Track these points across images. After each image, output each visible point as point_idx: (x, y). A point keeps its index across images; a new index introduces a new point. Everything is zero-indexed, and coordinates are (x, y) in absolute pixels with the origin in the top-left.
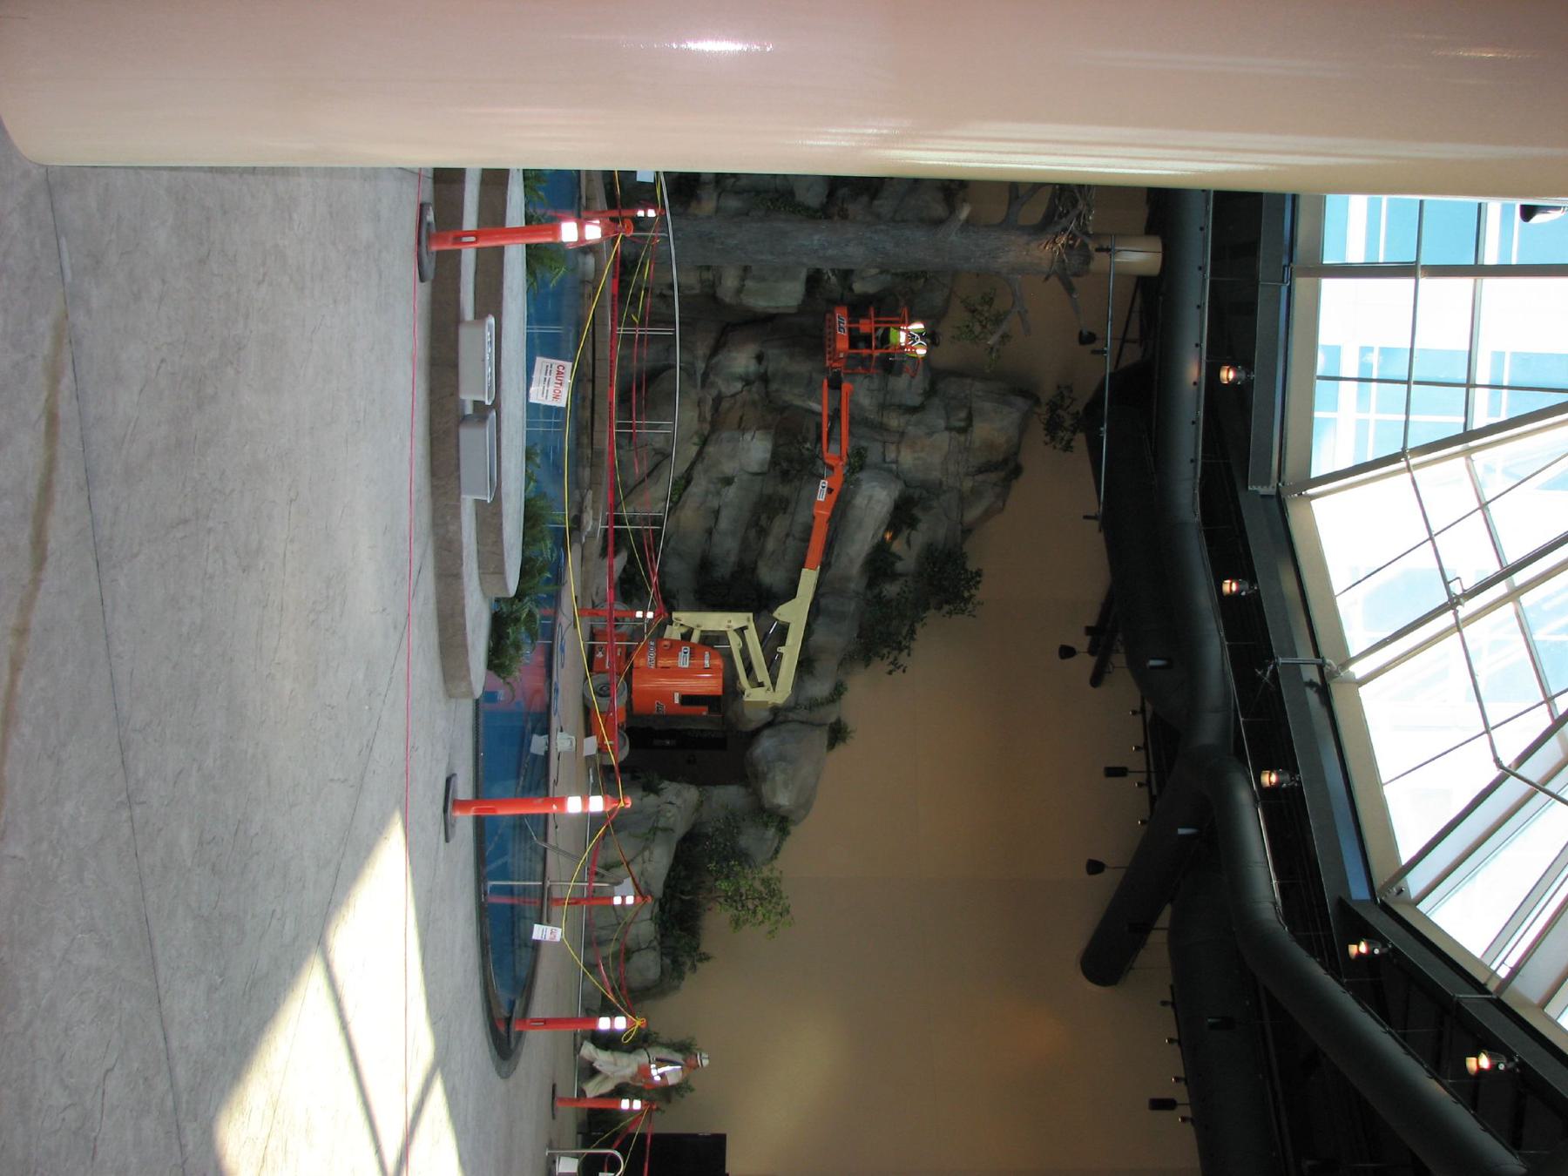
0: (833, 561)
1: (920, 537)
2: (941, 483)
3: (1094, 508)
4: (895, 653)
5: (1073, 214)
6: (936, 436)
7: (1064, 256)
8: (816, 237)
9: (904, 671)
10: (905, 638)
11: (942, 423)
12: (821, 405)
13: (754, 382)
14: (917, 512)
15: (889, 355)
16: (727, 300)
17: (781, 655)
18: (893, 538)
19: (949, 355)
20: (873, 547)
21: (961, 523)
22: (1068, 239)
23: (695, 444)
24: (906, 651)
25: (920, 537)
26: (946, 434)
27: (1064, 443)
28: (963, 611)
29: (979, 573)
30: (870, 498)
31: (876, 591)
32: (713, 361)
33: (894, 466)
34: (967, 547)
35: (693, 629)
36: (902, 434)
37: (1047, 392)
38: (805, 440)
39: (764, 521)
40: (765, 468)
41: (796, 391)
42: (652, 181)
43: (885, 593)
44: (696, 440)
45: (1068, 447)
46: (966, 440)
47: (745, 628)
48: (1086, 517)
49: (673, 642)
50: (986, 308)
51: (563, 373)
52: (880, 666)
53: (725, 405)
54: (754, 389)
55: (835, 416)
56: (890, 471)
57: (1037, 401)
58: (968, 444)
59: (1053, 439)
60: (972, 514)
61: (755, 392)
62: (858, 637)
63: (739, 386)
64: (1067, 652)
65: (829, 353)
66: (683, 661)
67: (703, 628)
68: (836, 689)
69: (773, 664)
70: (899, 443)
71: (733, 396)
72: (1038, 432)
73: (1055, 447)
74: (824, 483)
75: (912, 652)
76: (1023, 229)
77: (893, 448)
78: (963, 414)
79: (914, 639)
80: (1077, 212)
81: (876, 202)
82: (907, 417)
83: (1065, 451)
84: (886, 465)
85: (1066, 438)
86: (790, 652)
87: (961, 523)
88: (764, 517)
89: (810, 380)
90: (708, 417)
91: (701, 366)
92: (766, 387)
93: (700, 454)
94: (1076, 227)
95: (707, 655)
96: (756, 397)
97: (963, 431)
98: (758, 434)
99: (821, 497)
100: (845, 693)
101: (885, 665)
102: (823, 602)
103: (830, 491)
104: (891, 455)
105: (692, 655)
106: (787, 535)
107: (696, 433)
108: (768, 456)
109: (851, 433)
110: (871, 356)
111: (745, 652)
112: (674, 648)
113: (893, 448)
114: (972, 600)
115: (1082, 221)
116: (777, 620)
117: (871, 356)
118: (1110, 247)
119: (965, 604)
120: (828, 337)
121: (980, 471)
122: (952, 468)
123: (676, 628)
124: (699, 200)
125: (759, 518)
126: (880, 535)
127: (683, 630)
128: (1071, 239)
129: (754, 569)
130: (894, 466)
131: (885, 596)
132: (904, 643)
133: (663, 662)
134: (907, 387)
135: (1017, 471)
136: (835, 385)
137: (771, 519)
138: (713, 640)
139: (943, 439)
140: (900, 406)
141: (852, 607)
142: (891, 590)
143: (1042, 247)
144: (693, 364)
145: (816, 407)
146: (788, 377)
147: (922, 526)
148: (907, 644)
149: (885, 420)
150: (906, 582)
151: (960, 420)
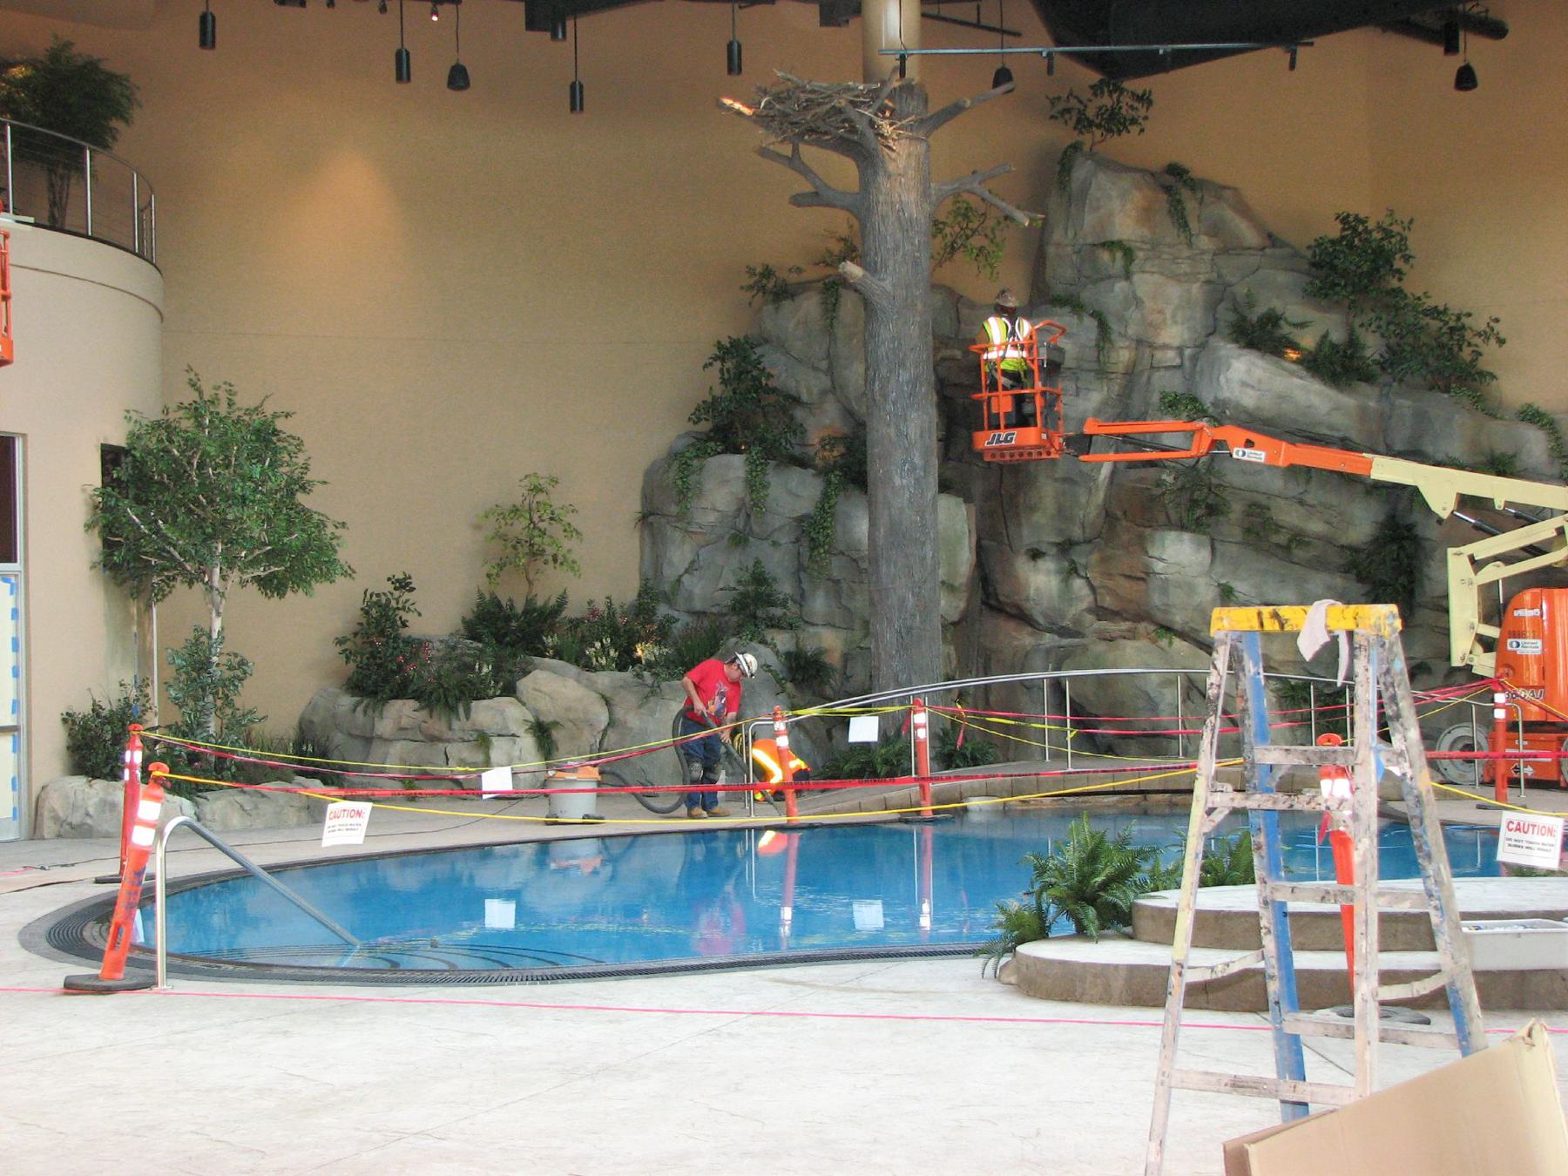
0: (1336, 434)
1: (1294, 309)
2: (1208, 282)
3: (1275, 56)
4: (1468, 335)
5: (852, 113)
6: (1140, 294)
7: (904, 122)
8: (897, 481)
9: (1497, 320)
10: (1446, 323)
11: (1120, 286)
12: (1104, 463)
13: (1073, 562)
14: (1254, 316)
15: (1040, 367)
16: (962, 605)
17: (1508, 504)
18: (1295, 347)
19: (1014, 282)
20: (1313, 376)
21: (1264, 248)
22: (884, 118)
23: (1171, 643)
24: (1464, 320)
25: (1294, 309)
26: (1136, 278)
27: (1136, 105)
28: (1403, 239)
29: (1344, 220)
30: (1244, 384)
31: (1376, 369)
32: (1041, 620)
33: (1188, 352)
34: (1301, 239)
35: (1477, 635)
36: (1139, 342)
37: (1062, 135)
38: (1159, 483)
39: (1282, 539)
40: (1205, 539)
41: (1083, 500)
42: (877, 718)
43: (1377, 357)
44: (1164, 642)
45: (1145, 99)
46: (1141, 249)
47: (1472, 559)
48: (1292, 66)
49: (1500, 663)
50: (948, 230)
51: (1519, 824)
52: (1491, 358)
53: (1108, 601)
54: (1083, 561)
55: (1127, 441)
56: (1194, 359)
57: (1076, 147)
58: (1145, 247)
59: (1134, 121)
60: (1250, 236)
61: (1086, 558)
62: (1449, 392)
63: (1078, 584)
64: (1466, 79)
65: (1040, 454)
66: (1530, 647)
67: (1476, 620)
68: (1531, 421)
69: (1526, 516)
70: (1152, 346)
71: (1093, 589)
72: (1117, 145)
73: (1146, 118)
74: (1238, 452)
75: (1465, 311)
76: (866, 183)
77: (1159, 355)
78: (1105, 256)
79: (1446, 309)
80: (850, 107)
81: (805, 397)
82: (1114, 337)
83: (1150, 103)
84: (1187, 364)
85: (1130, 103)
86: (1501, 491)
87: (1264, 248)
88: (1275, 539)
89: (1067, 480)
90: (1125, 625)
91: (1048, 639)
92: (1078, 543)
93: (1182, 635)
94: (870, 106)
95: (1516, 613)
96: (1095, 557)
97: (1128, 253)
98: (1154, 551)
99: (1257, 456)
100: (1535, 406)
101: (1490, 349)
102: (1399, 447)
103: (1249, 444)
104: (1171, 357)
105: (1519, 634)
106: (1301, 503)
107: (1154, 642)
108: (1186, 536)
109: (1142, 417)
110: (1043, 393)
111: (1507, 559)
112: (1510, 665)
113: (1159, 355)
114: (1384, 226)
115: (862, 99)
116: (1452, 512)
117: (1043, 393)
118: (898, 57)
119: (1393, 236)
120: (1008, 458)
121: (1183, 225)
122: (1185, 267)
123: (1476, 659)
124: (821, 652)
125: (1278, 546)
126: (1294, 367)
127: (1479, 649)
128: (884, 113)
129: (1354, 550)
130: (1188, 352)
131: (1381, 356)
132: (1452, 324)
133: (1533, 675)
134: (1076, 338)
135: (1175, 171)
136: (1082, 443)
137: (1278, 528)
138: (1495, 608)
139: (1144, 283)
140: (1099, 349)
141: (1405, 404)
142: (1373, 346)
143: (893, 155)
144: (1048, 651)
145: (1105, 471)
146: (1063, 514)
147: (1277, 305)
148: (1454, 318)
149: (1121, 368)
150: (1362, 325)
151: (1114, 260)
